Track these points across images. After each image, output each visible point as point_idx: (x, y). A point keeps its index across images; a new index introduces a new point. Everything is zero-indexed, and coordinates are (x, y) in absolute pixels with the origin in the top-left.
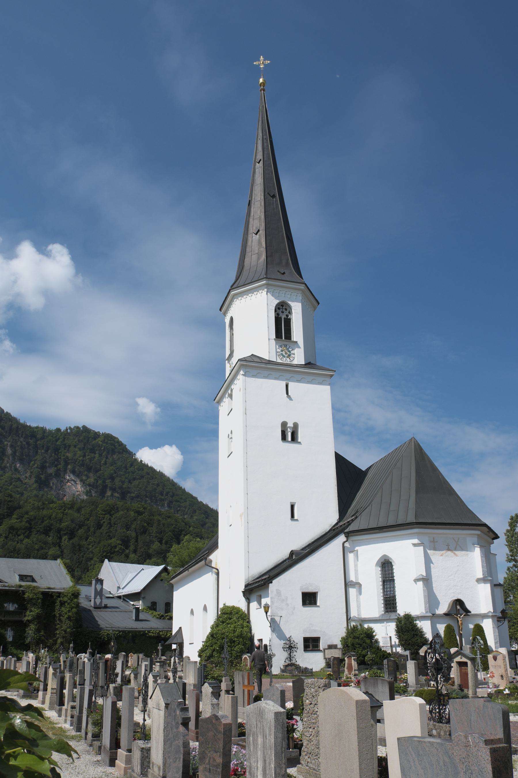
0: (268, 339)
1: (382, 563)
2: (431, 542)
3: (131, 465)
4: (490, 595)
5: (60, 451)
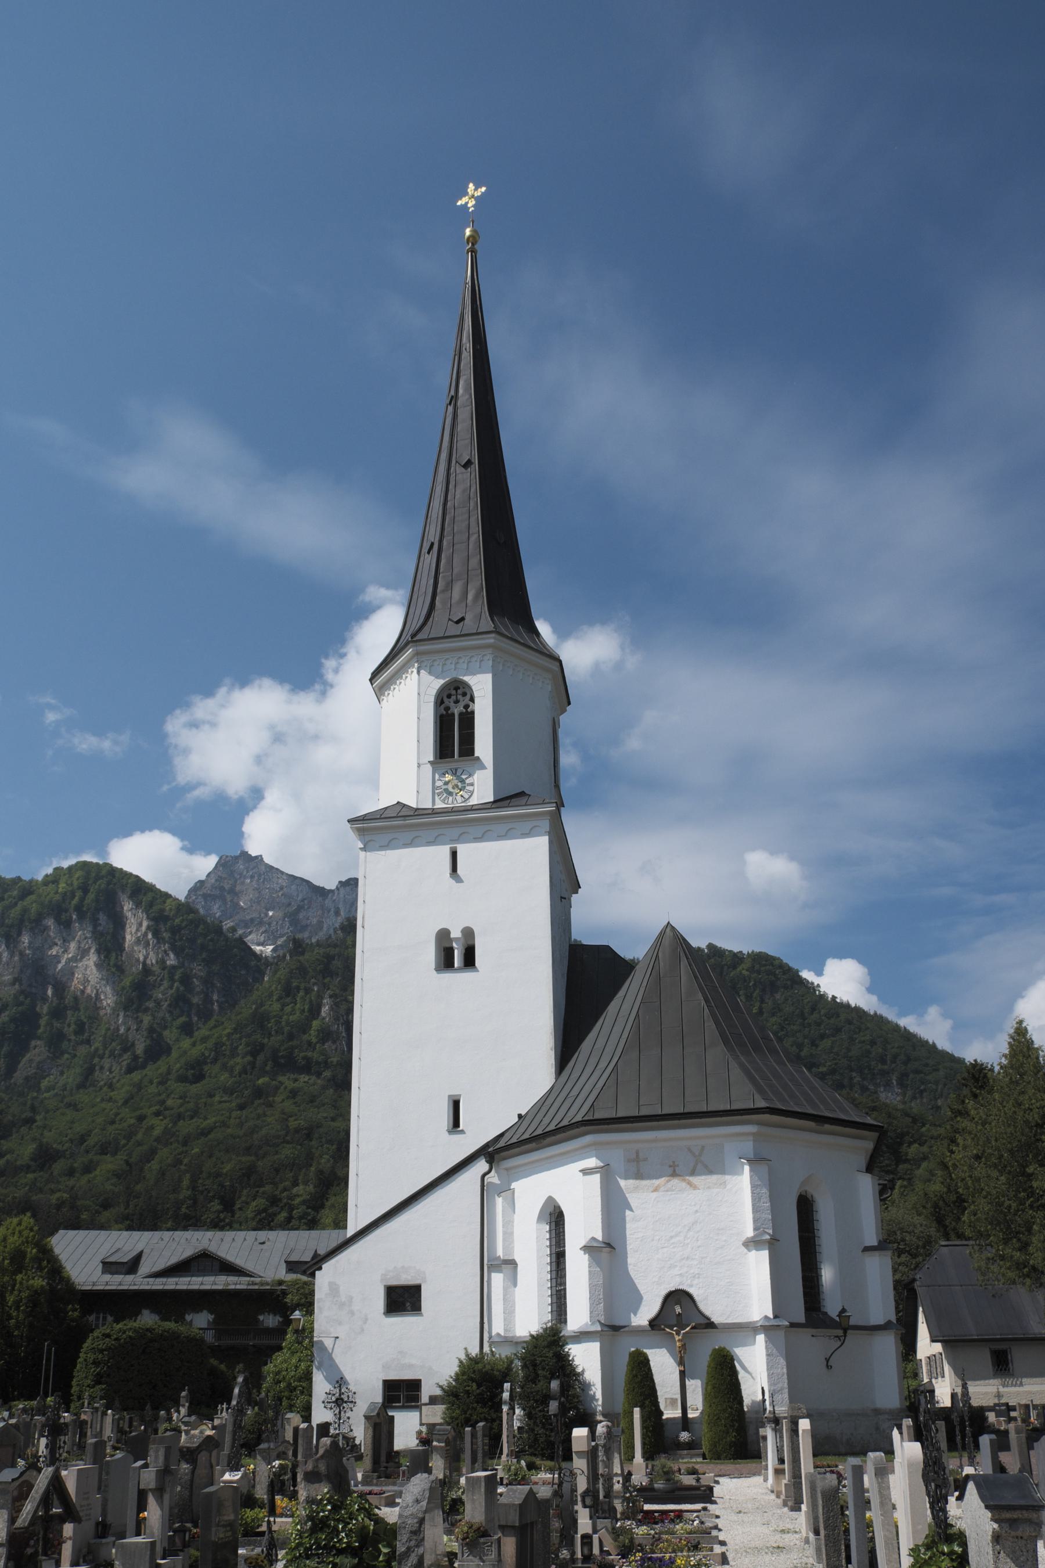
0: (416, 765)
1: (550, 1214)
2: (629, 1161)
3: (813, 1009)
4: (769, 1277)
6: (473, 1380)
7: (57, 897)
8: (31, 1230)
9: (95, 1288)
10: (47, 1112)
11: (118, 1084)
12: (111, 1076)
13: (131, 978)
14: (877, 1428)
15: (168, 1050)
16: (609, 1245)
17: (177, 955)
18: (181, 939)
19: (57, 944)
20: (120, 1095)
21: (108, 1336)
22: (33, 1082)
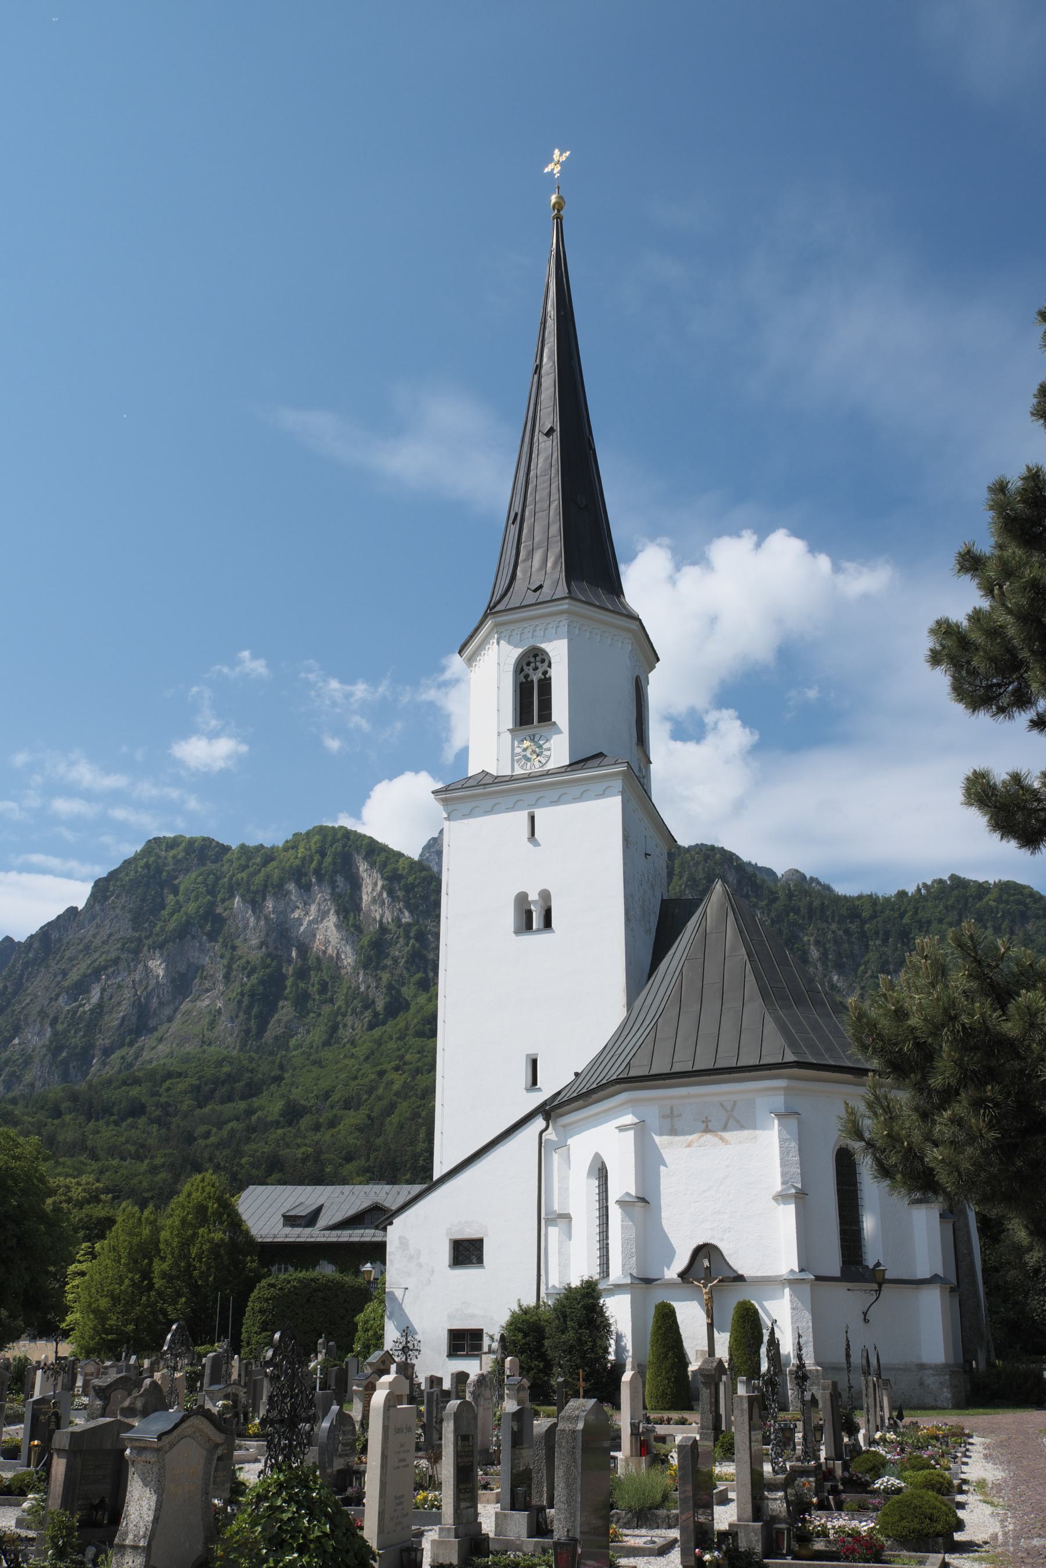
2: (664, 1117)
4: (795, 1230)
5: (911, 936)
6: (520, 1330)
7: (297, 862)
8: (213, 1186)
9: (276, 1240)
10: (294, 1069)
11: (360, 1041)
12: (354, 1033)
13: (369, 937)
14: (922, 1384)
15: (407, 1006)
16: (643, 1200)
17: (410, 912)
18: (415, 897)
19: (298, 908)
20: (361, 1051)
21: (273, 1286)
22: (282, 1041)
